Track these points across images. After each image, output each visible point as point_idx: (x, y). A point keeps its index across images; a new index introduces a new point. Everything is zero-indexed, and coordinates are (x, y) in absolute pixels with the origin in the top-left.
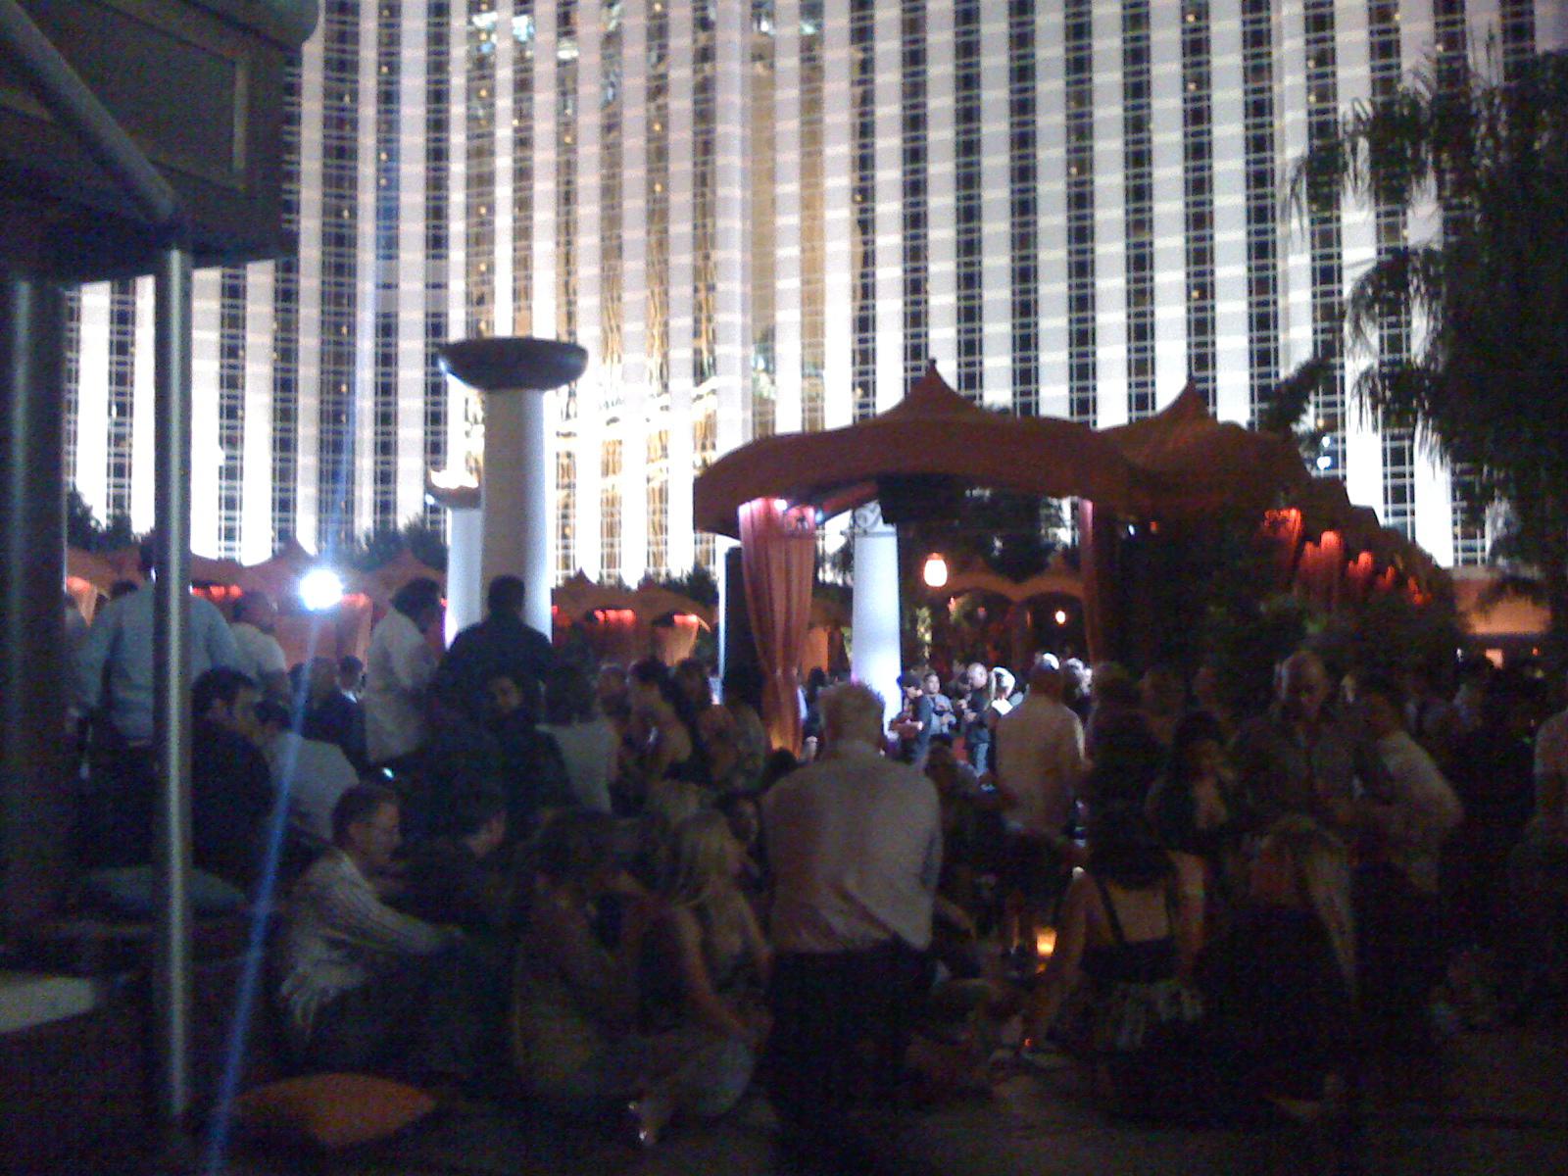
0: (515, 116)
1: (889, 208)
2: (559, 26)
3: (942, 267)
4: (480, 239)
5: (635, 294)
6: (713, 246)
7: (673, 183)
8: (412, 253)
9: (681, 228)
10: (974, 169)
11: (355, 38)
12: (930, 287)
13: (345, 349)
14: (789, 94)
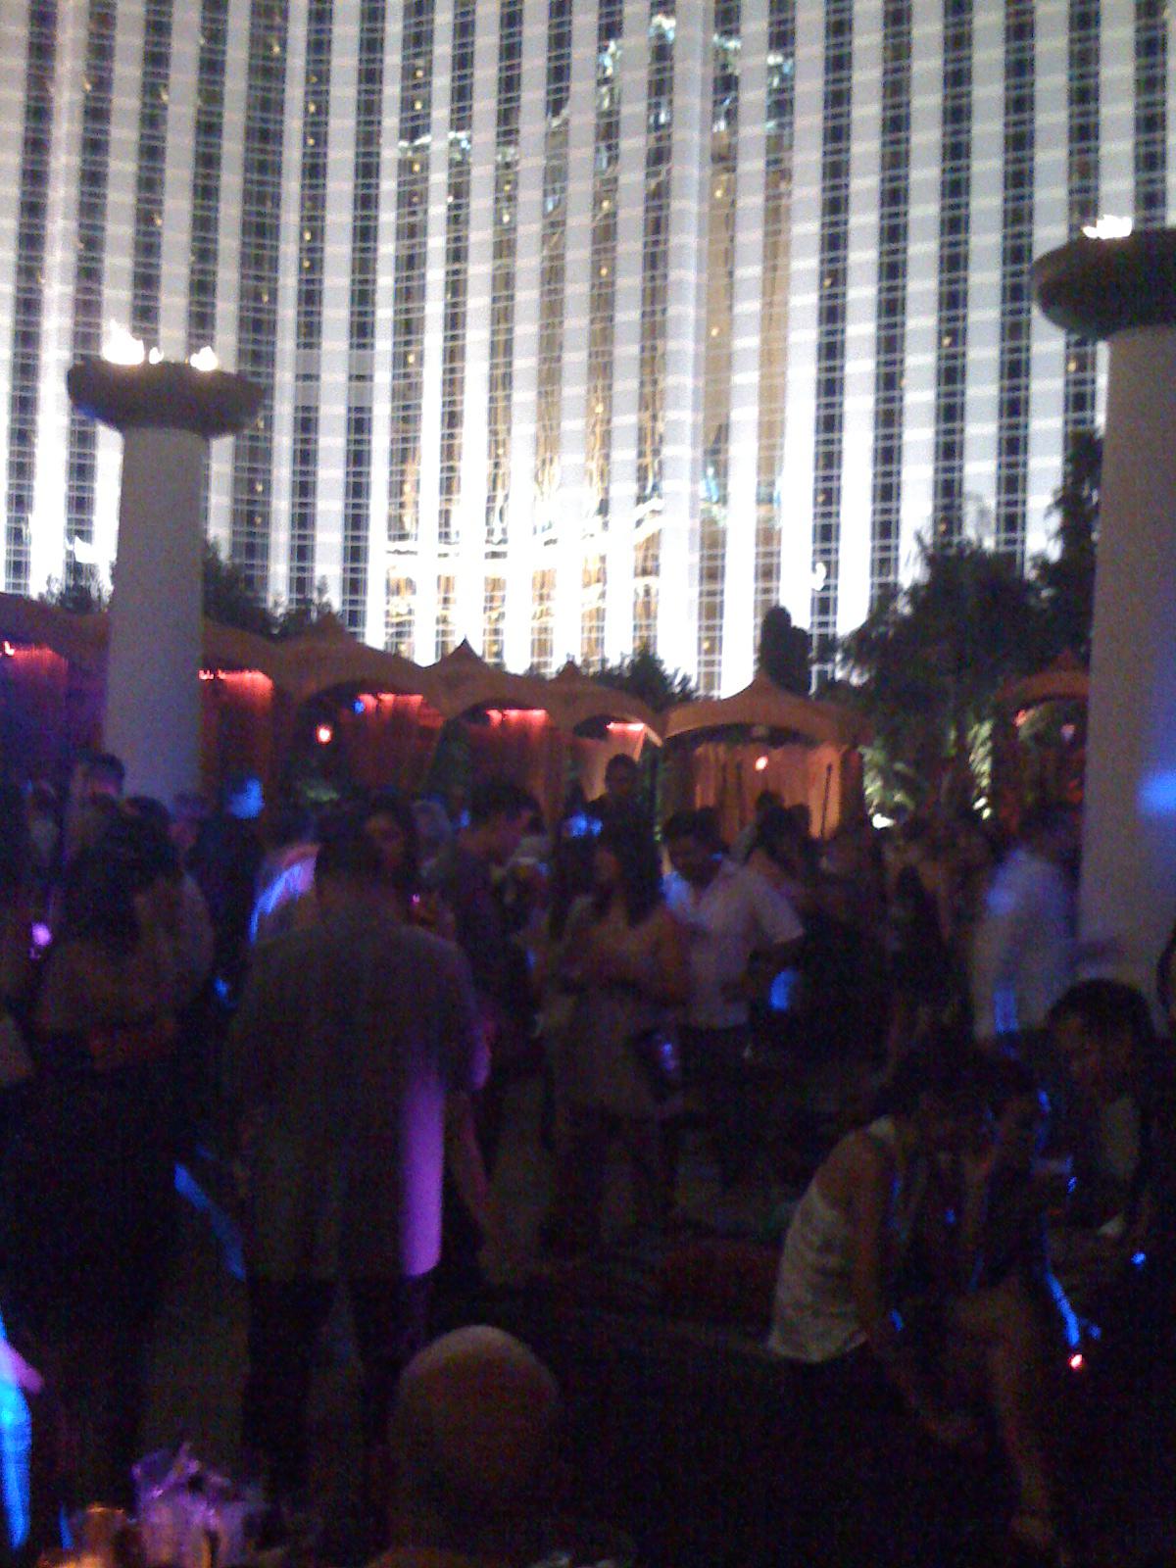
0: (449, 193)
1: (863, 256)
2: (500, 92)
3: (925, 174)
4: (408, 328)
5: (574, 389)
6: (664, 369)
7: (621, 265)
8: (335, 341)
9: (628, 315)
10: (961, 249)
11: (280, 107)
12: (905, 382)
13: (261, 444)
14: (751, 201)
